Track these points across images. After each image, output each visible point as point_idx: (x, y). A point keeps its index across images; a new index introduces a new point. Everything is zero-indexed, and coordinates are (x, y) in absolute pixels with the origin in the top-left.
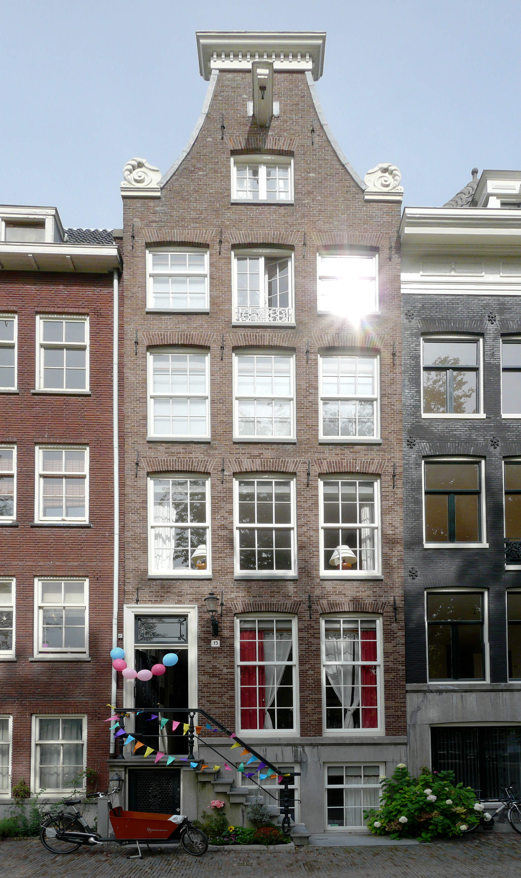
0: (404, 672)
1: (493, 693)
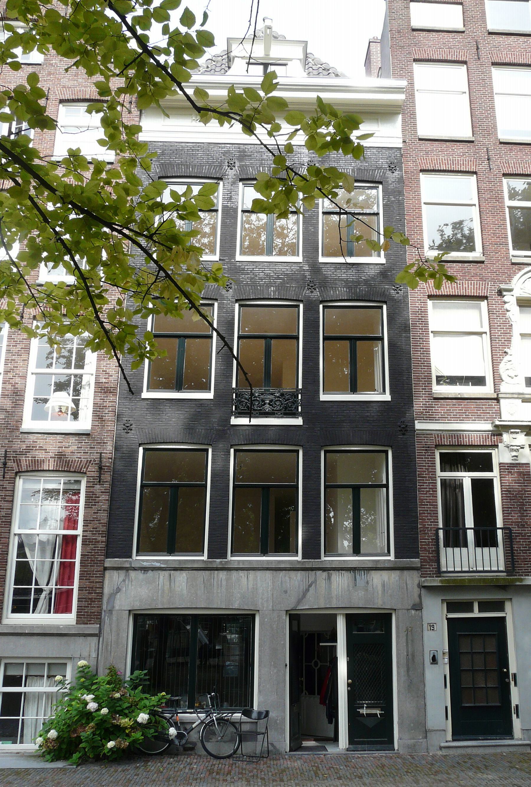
0: (103, 545)
1: (207, 572)
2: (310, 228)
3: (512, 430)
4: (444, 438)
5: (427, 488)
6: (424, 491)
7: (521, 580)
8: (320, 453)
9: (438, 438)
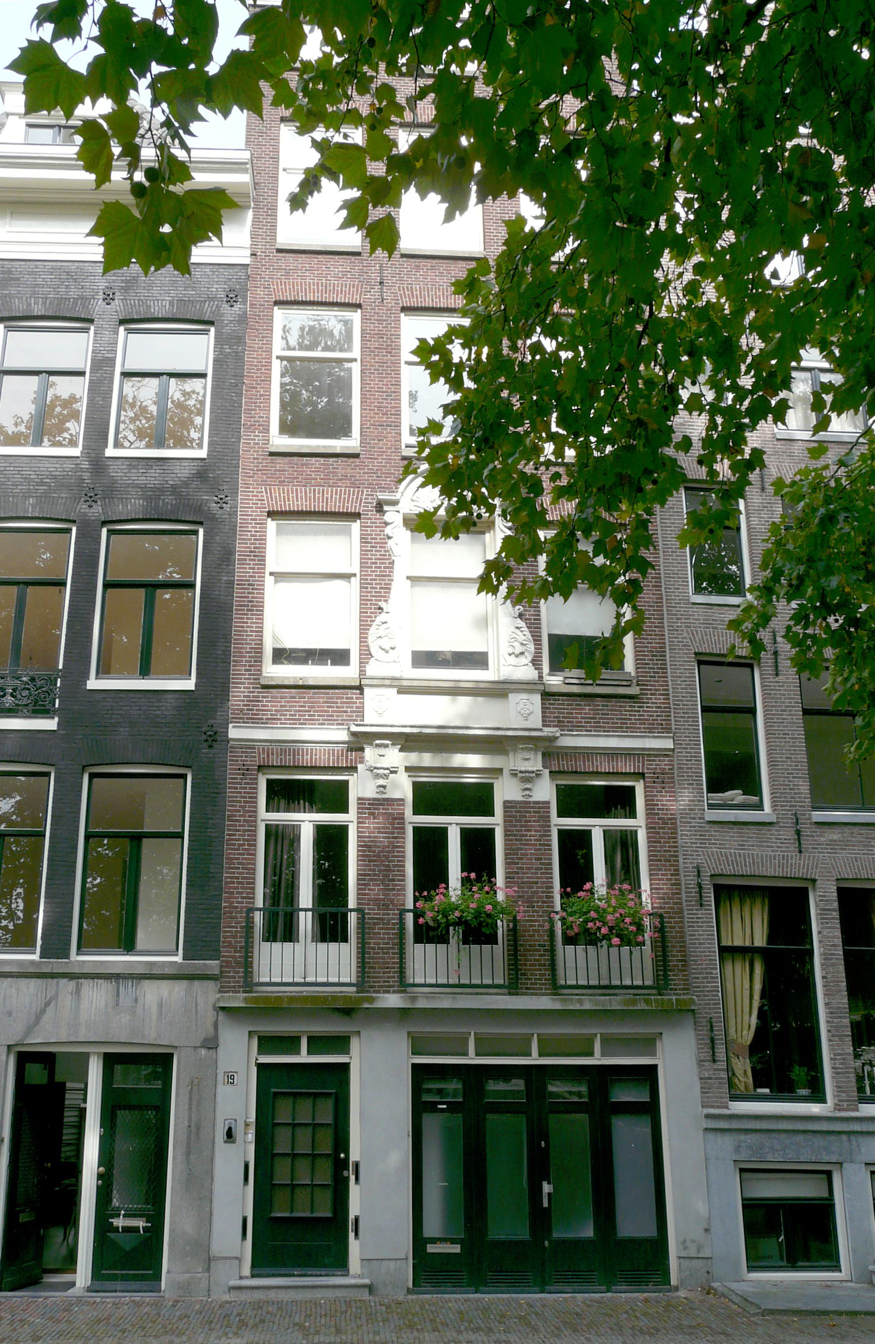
2: (98, 399)
3: (378, 742)
4: (273, 754)
5: (239, 840)
6: (234, 845)
7: (372, 1000)
8: (82, 779)
9: (264, 753)
